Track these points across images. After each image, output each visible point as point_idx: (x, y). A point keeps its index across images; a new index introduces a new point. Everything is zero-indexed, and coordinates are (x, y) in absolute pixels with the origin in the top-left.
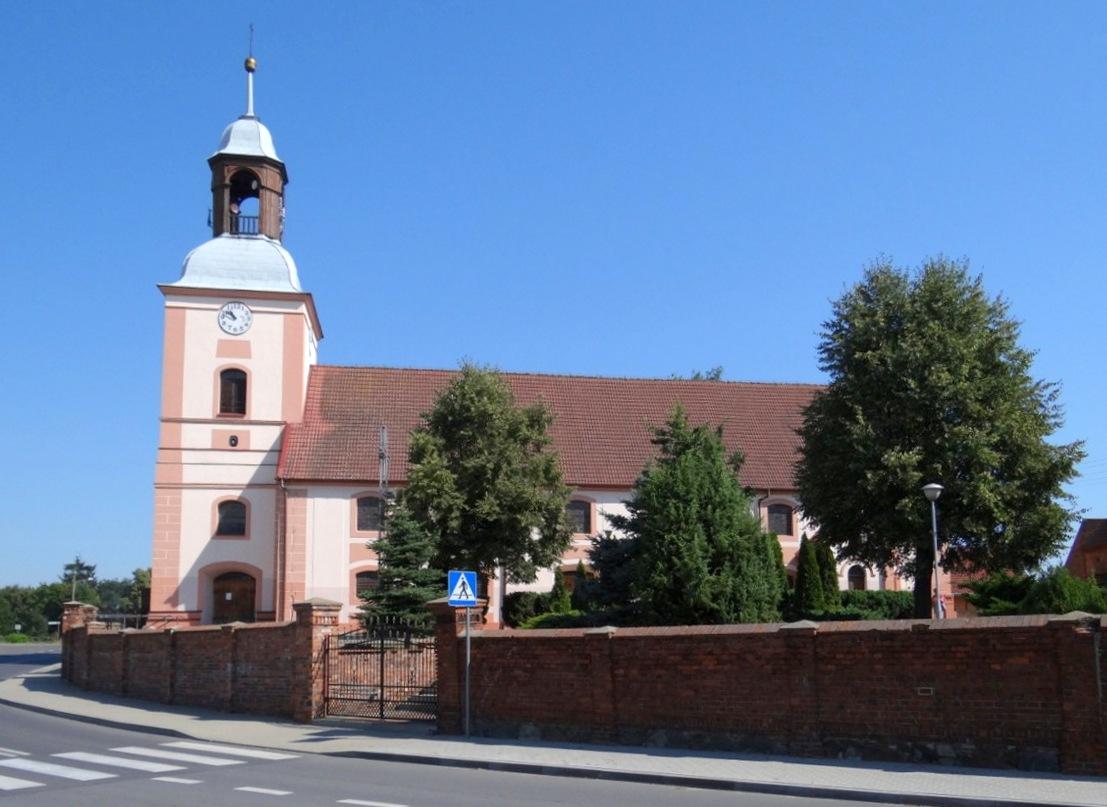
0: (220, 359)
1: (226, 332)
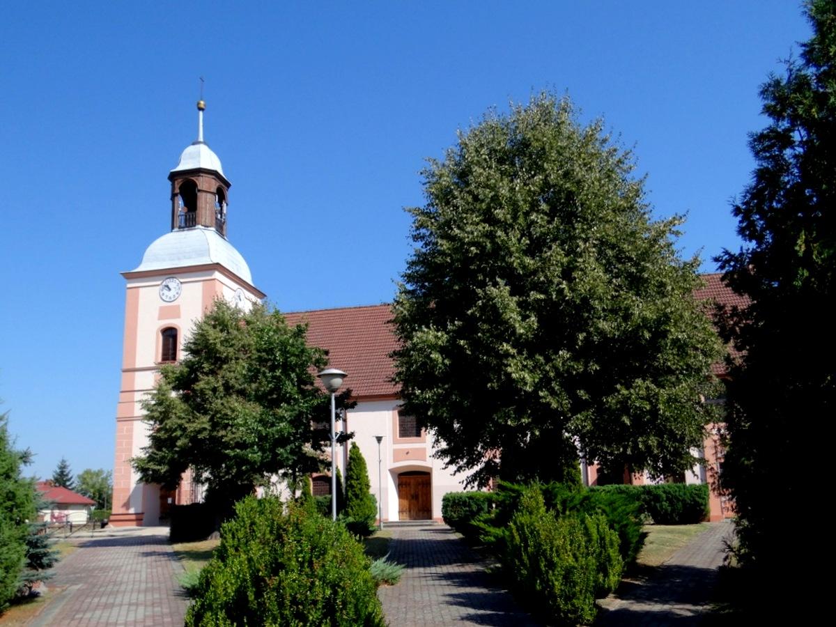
0: (160, 321)
1: (163, 300)
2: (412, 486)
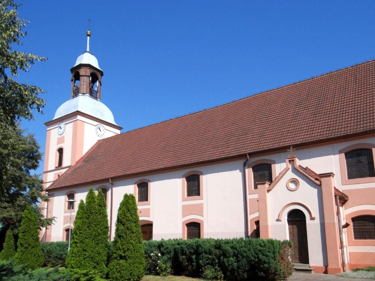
2: (148, 234)
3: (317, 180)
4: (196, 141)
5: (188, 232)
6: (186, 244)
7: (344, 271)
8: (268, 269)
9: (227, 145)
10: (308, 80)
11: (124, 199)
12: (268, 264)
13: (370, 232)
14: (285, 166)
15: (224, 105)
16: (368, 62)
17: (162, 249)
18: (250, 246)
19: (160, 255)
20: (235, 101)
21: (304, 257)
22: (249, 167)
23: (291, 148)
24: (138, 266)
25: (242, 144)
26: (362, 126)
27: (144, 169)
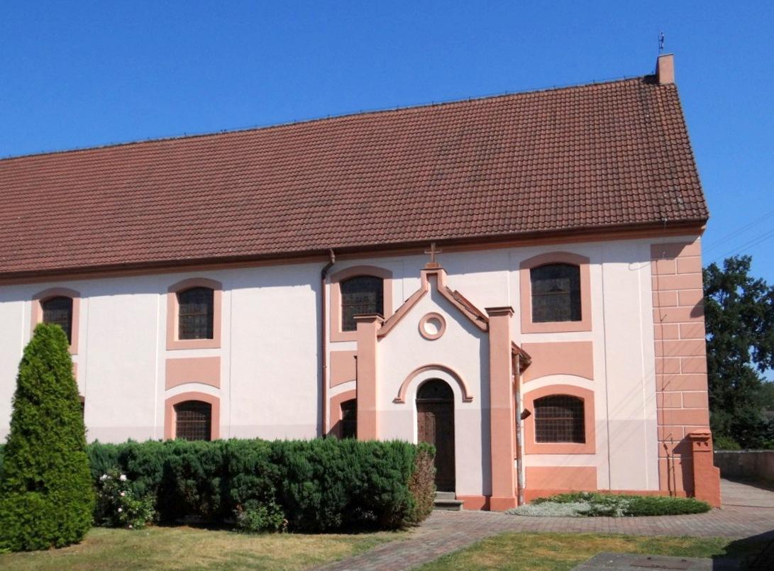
3: (480, 323)
4: (203, 207)
5: (178, 424)
6: (196, 452)
7: (519, 504)
8: (389, 504)
9: (282, 224)
10: (462, 102)
11: (35, 337)
12: (390, 494)
13: (564, 427)
14: (419, 286)
15: (274, 127)
16: (577, 87)
17: (131, 464)
18: (354, 455)
19: (123, 477)
20: (299, 123)
21: (446, 480)
22: (333, 281)
23: (433, 246)
24: (78, 506)
25: (318, 225)
26: (565, 217)
27: (63, 263)
